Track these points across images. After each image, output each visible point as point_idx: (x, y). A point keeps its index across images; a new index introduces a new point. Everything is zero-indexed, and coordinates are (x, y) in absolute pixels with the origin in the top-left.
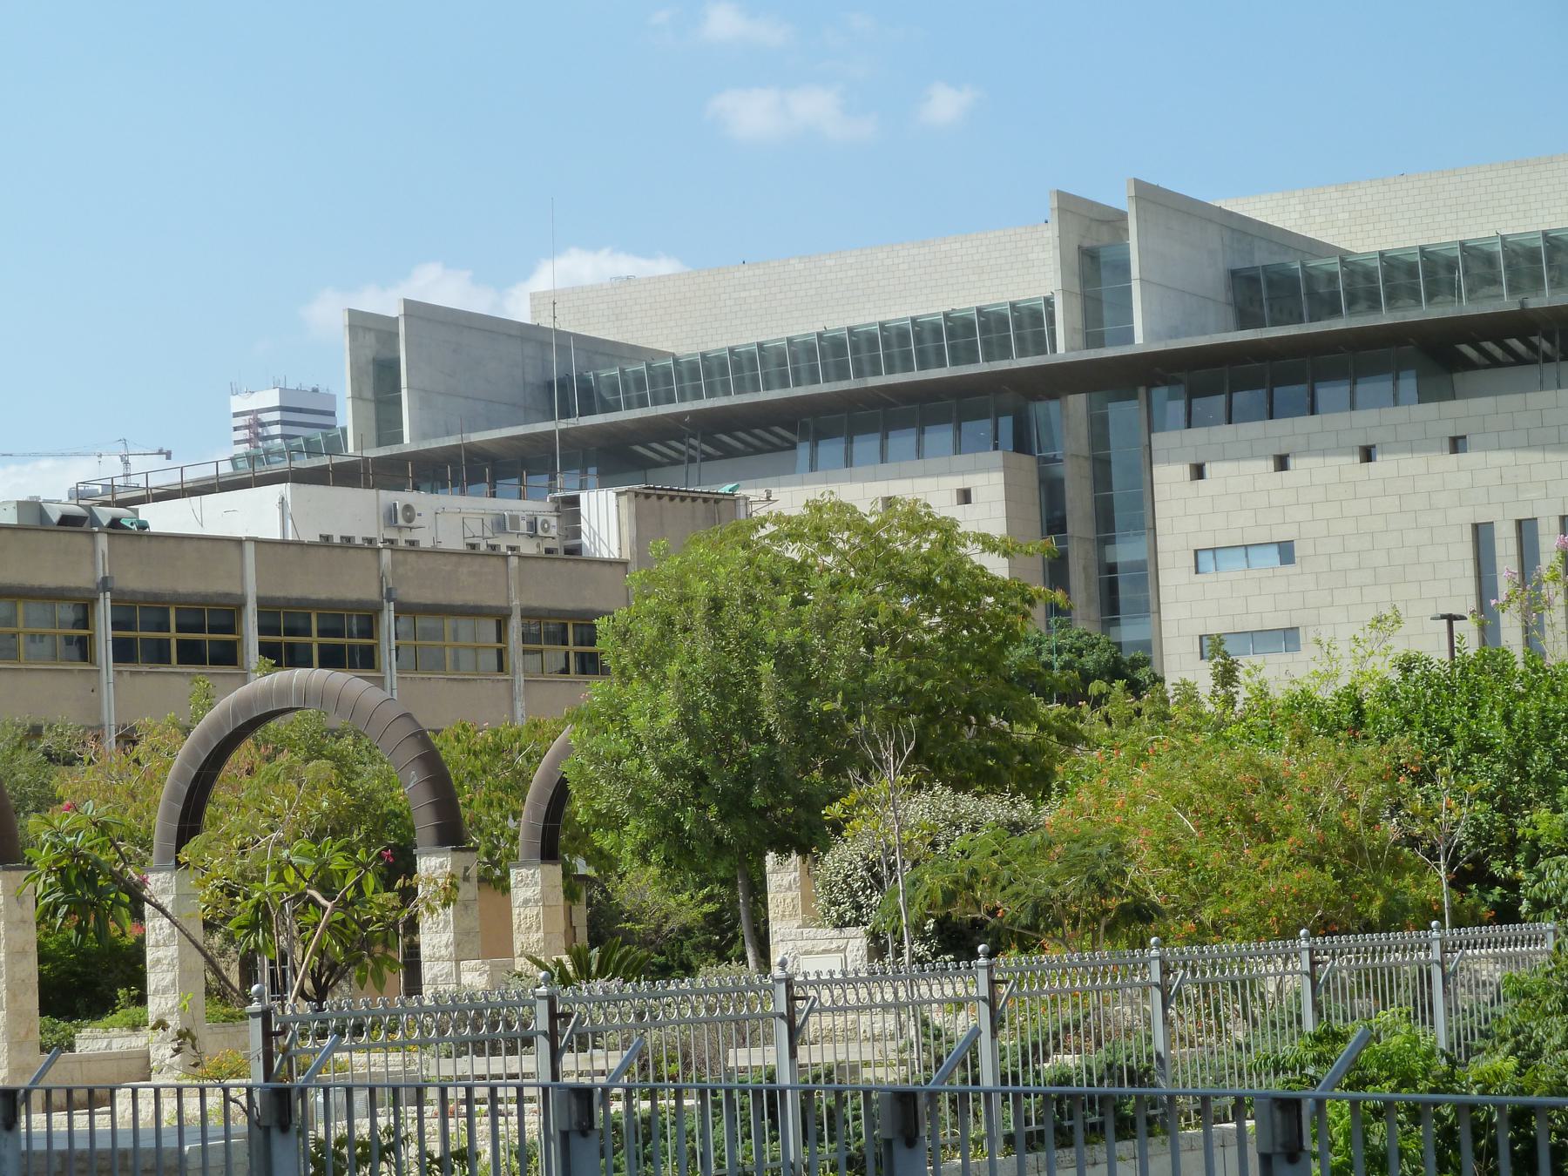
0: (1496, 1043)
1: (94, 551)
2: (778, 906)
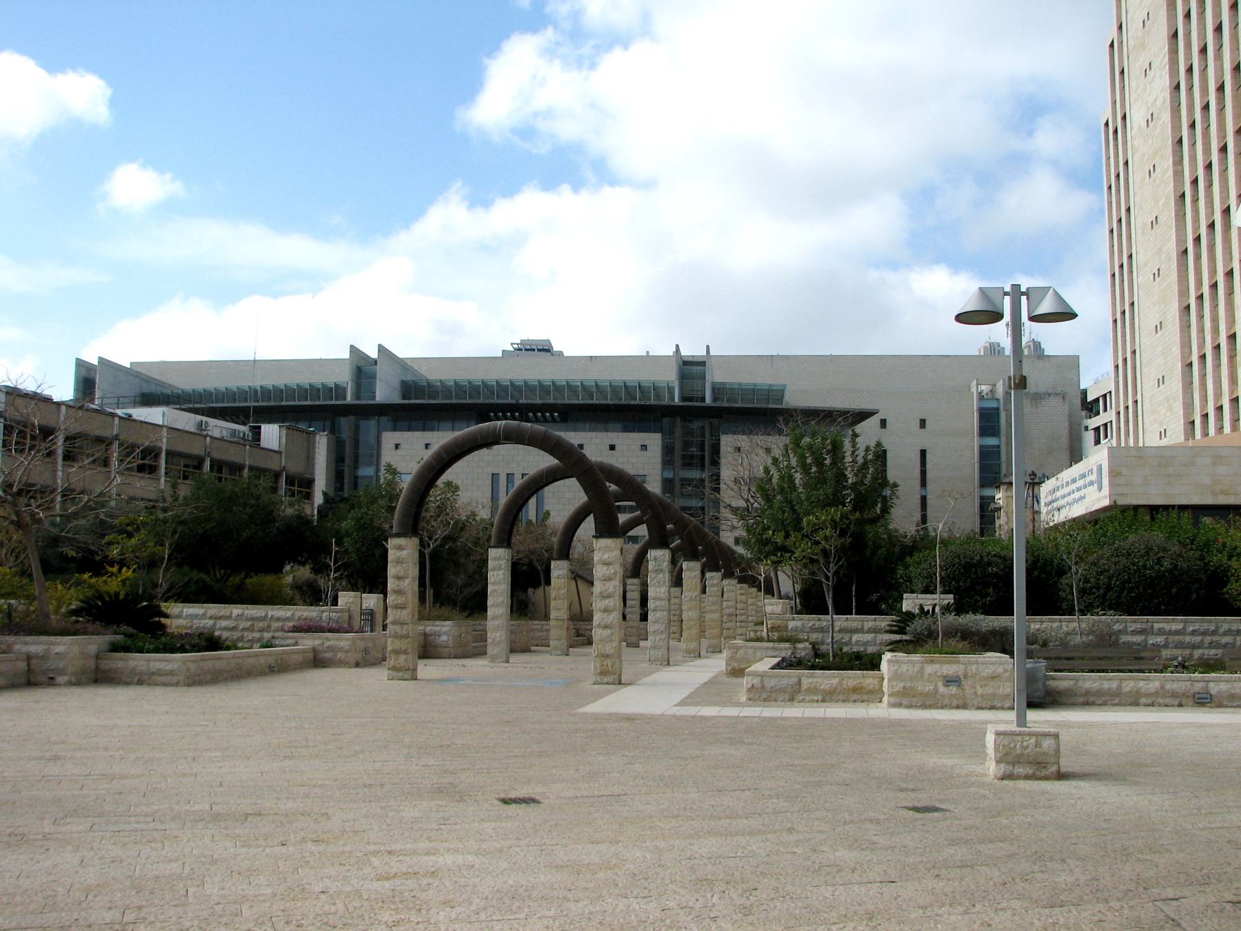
1: (113, 424)
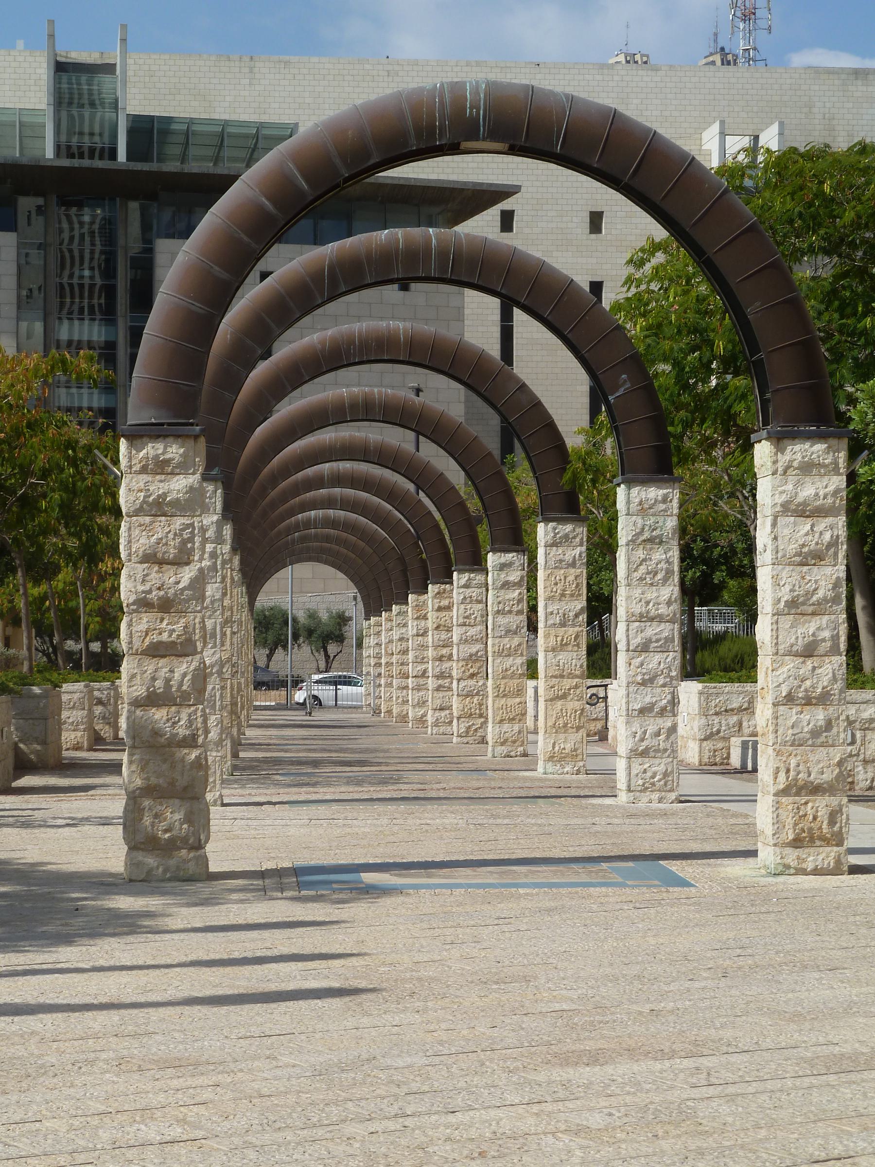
0: (134, 620)
2: (556, 584)
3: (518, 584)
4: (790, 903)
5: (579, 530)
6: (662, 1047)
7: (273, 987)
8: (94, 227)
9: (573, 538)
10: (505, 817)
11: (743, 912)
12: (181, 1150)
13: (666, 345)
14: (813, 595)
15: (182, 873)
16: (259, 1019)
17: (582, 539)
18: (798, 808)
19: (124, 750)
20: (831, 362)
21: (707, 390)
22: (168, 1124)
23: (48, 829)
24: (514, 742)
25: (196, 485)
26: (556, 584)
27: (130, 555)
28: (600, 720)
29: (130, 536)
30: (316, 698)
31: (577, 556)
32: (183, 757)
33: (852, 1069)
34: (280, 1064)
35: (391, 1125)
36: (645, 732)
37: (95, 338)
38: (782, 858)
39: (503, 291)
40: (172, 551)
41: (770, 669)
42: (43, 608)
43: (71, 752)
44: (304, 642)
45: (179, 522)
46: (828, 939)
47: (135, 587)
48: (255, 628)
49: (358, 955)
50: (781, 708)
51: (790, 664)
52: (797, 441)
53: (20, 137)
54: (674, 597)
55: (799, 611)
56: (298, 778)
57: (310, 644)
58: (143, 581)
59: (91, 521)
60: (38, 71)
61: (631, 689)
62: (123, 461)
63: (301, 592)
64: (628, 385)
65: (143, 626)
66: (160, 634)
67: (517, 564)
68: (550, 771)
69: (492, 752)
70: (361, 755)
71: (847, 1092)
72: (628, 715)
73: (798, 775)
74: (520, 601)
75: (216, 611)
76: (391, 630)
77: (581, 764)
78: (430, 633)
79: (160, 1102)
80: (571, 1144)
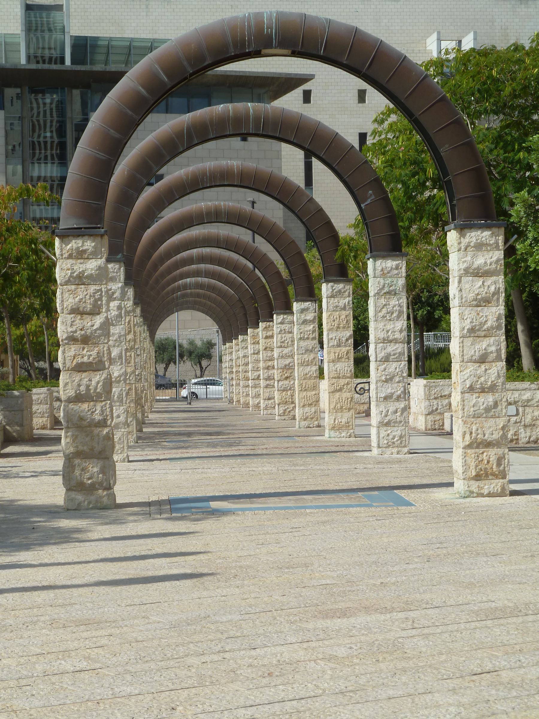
0: (66, 349)
2: (334, 321)
3: (313, 321)
4: (472, 515)
5: (347, 287)
6: (386, 606)
7: (150, 574)
8: (52, 106)
9: (343, 292)
10: (301, 465)
11: (443, 521)
12: (85, 676)
13: (397, 172)
14: (484, 325)
15: (99, 504)
16: (140, 594)
17: (349, 292)
18: (478, 456)
19: (62, 429)
20: (499, 180)
21: (424, 199)
22: (78, 660)
23: (20, 479)
24: (312, 418)
25: (103, 265)
26: (334, 321)
27: (63, 309)
28: (366, 403)
29: (62, 297)
30: (193, 393)
31: (347, 303)
32: (99, 433)
33: (502, 616)
34: (151, 621)
35: (215, 658)
36: (388, 411)
37: (55, 174)
38: (468, 487)
39: (295, 141)
40: (89, 306)
41: (459, 371)
42: (23, 342)
43: (40, 430)
44: (187, 359)
45: (92, 288)
46: (494, 536)
47: (66, 329)
48: (156, 352)
49: (204, 553)
50: (466, 395)
51: (471, 367)
52: (472, 230)
53: (5, 51)
54: (404, 327)
55: (476, 335)
56: (177, 444)
57: (191, 360)
58: (71, 325)
59: (47, 288)
60: (16, 10)
61: (379, 385)
62: (57, 251)
63: (185, 329)
64: (373, 197)
65: (72, 353)
66: (83, 357)
67: (311, 309)
68: (333, 436)
69: (298, 425)
70: (218, 429)
71: (497, 631)
72: (377, 401)
73: (477, 435)
74: (314, 332)
75: (122, 342)
76: (239, 351)
77: (352, 431)
78: (261, 352)
79: (75, 646)
80: (325, 667)
